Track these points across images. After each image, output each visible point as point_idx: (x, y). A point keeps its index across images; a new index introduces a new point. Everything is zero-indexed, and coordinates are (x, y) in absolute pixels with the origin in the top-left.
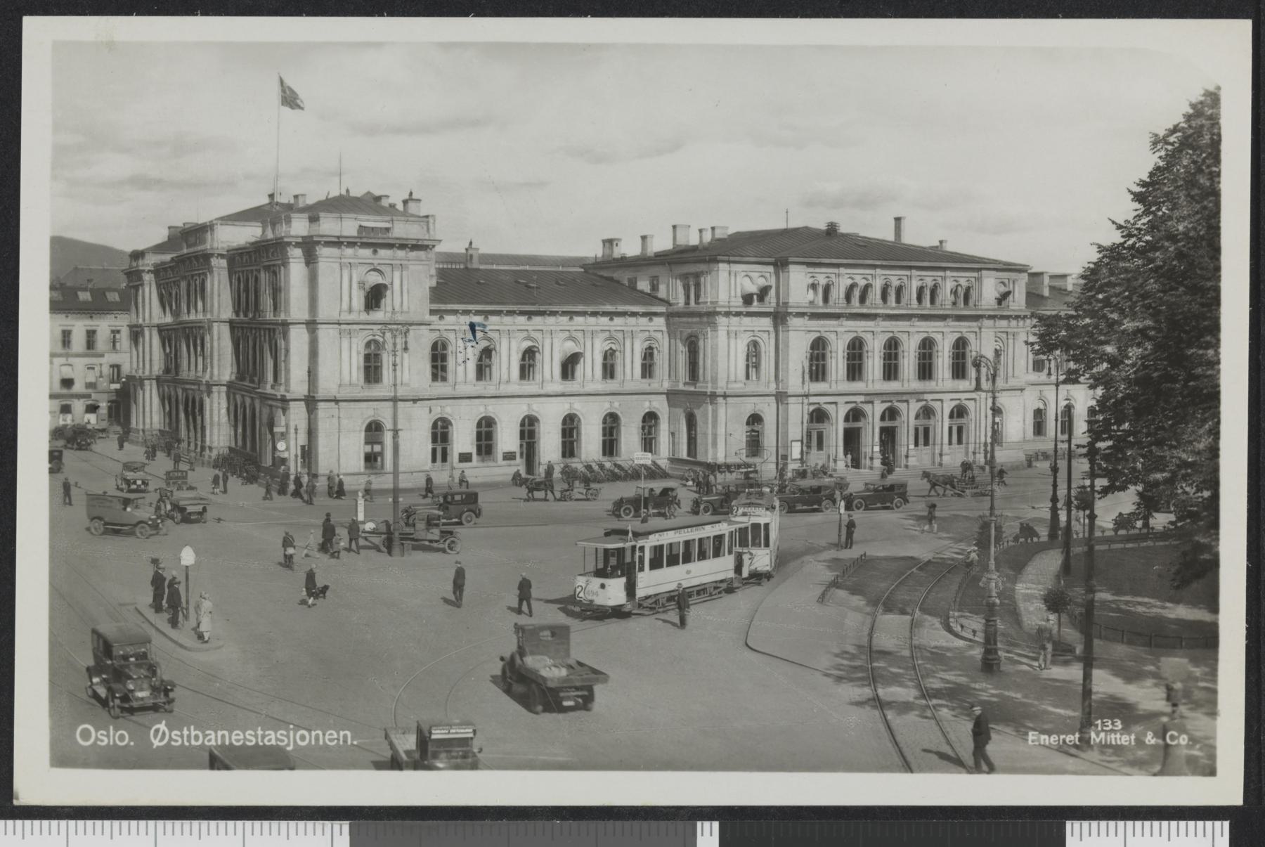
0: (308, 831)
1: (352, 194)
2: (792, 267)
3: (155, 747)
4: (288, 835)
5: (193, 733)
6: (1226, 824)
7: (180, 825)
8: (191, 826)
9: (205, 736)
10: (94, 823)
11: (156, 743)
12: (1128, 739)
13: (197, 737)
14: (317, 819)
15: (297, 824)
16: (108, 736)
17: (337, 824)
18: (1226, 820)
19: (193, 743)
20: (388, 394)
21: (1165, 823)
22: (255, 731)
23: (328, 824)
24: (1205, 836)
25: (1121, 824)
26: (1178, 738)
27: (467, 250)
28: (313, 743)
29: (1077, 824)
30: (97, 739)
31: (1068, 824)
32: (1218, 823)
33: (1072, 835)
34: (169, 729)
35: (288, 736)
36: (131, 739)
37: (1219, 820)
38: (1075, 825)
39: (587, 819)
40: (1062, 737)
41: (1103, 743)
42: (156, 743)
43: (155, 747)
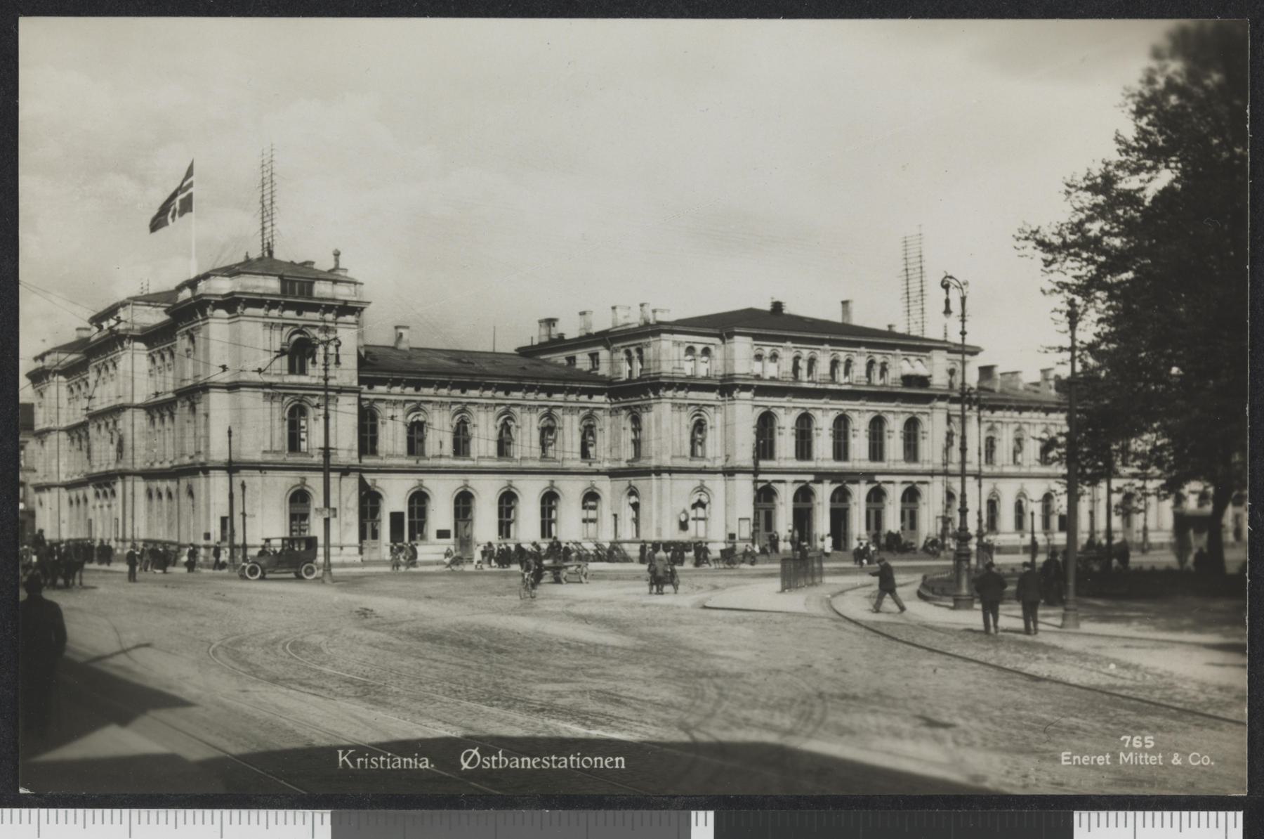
0: (279, 821)
2: (737, 338)
3: (463, 769)
4: (267, 825)
6: (1240, 814)
7: (155, 814)
8: (167, 815)
9: (510, 762)
10: (66, 812)
11: (465, 766)
12: (1103, 759)
15: (277, 813)
17: (318, 813)
18: (1240, 810)
20: (630, 449)
21: (1176, 814)
23: (309, 812)
24: (1217, 827)
25: (1130, 814)
29: (1085, 814)
31: (1076, 814)
32: (1231, 814)
33: (1080, 826)
34: (480, 754)
37: (1232, 810)
38: (1082, 815)
39: (577, 809)
42: (465, 766)
43: (463, 769)
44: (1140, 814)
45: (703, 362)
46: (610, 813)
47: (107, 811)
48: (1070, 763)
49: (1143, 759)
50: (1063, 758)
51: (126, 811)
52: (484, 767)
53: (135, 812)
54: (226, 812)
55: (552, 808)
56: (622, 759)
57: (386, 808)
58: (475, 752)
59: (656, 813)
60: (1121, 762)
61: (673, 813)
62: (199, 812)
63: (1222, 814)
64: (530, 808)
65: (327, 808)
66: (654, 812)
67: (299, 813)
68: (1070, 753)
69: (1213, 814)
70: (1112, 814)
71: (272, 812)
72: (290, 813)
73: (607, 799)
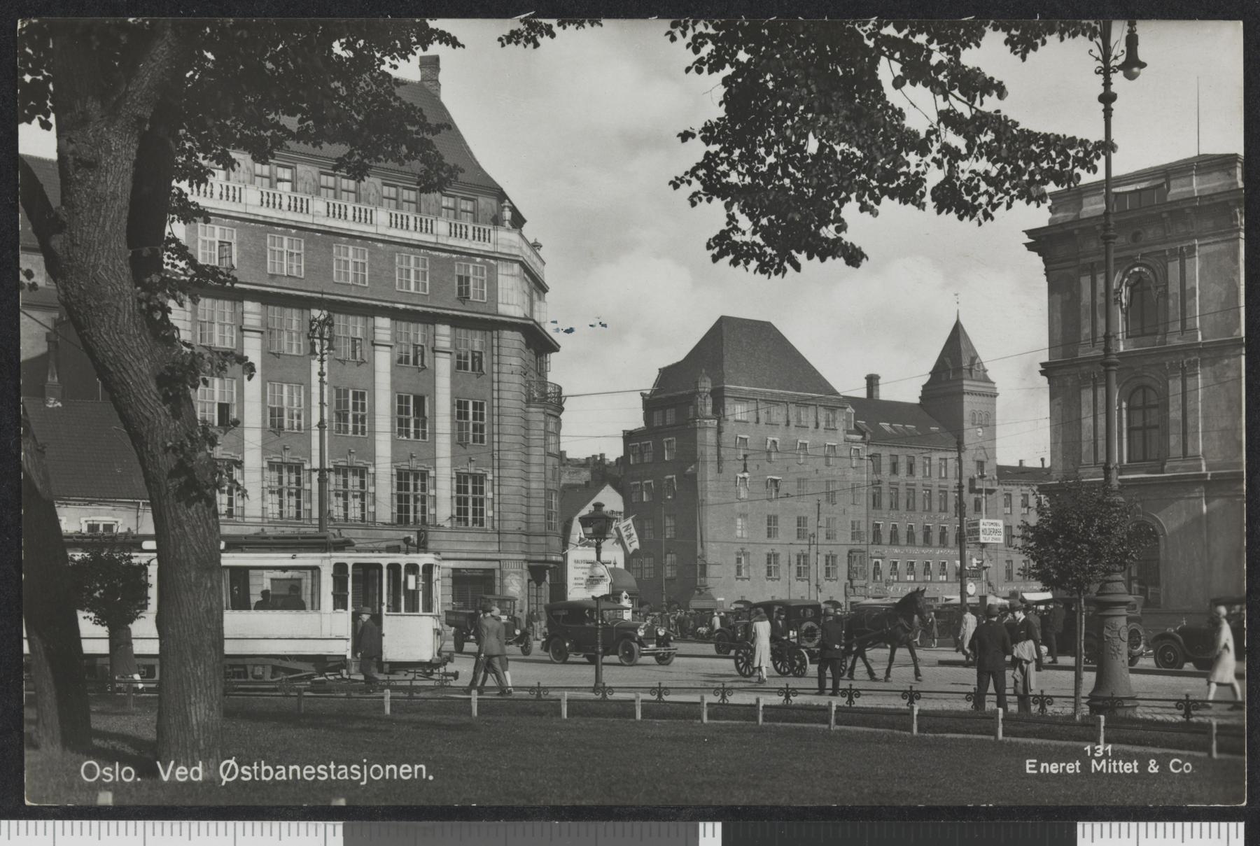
1: (665, 25)
5: (264, 768)
6: (1242, 825)
9: (276, 771)
12: (1131, 766)
13: (267, 772)
14: (310, 820)
16: (113, 773)
17: (330, 825)
19: (264, 778)
21: (1178, 825)
22: (328, 765)
23: (321, 824)
25: (1133, 825)
26: (1181, 766)
27: (1132, 65)
28: (291, 777)
29: (1088, 825)
30: (240, 774)
31: (1080, 825)
32: (1233, 825)
35: (361, 771)
36: (137, 775)
37: (1234, 821)
38: (328, 827)
40: (1062, 765)
41: (1104, 771)
44: (1142, 825)
45: (1026, 496)
46: (619, 824)
47: (122, 823)
48: (1035, 772)
49: (1117, 767)
50: (1028, 766)
51: (140, 823)
52: (319, 778)
53: (149, 823)
54: (239, 824)
55: (562, 819)
56: (423, 767)
57: (398, 819)
58: (232, 762)
59: (664, 825)
60: (1093, 771)
61: (681, 824)
62: (212, 824)
63: (1224, 825)
64: (540, 820)
65: (339, 820)
66: (662, 823)
67: (312, 824)
68: (1035, 761)
69: (1215, 825)
70: (1115, 825)
71: (285, 824)
72: (303, 824)
73: (616, 810)
